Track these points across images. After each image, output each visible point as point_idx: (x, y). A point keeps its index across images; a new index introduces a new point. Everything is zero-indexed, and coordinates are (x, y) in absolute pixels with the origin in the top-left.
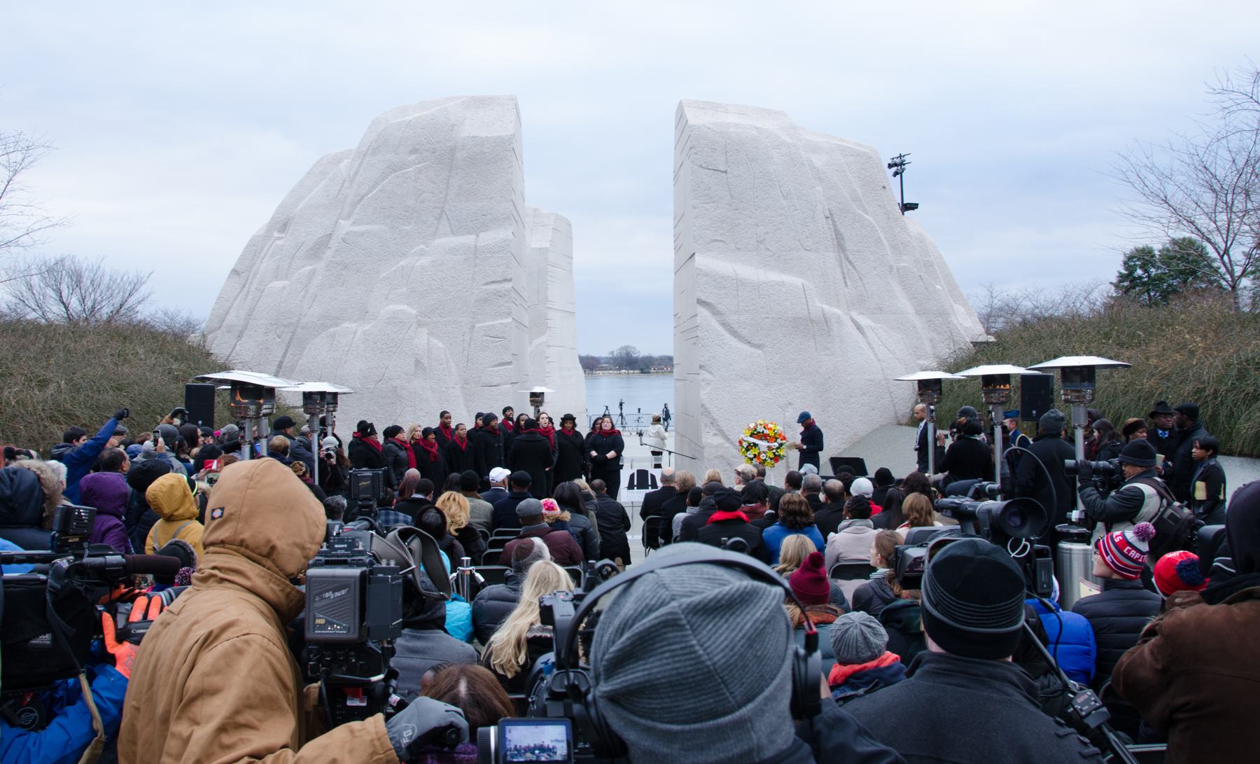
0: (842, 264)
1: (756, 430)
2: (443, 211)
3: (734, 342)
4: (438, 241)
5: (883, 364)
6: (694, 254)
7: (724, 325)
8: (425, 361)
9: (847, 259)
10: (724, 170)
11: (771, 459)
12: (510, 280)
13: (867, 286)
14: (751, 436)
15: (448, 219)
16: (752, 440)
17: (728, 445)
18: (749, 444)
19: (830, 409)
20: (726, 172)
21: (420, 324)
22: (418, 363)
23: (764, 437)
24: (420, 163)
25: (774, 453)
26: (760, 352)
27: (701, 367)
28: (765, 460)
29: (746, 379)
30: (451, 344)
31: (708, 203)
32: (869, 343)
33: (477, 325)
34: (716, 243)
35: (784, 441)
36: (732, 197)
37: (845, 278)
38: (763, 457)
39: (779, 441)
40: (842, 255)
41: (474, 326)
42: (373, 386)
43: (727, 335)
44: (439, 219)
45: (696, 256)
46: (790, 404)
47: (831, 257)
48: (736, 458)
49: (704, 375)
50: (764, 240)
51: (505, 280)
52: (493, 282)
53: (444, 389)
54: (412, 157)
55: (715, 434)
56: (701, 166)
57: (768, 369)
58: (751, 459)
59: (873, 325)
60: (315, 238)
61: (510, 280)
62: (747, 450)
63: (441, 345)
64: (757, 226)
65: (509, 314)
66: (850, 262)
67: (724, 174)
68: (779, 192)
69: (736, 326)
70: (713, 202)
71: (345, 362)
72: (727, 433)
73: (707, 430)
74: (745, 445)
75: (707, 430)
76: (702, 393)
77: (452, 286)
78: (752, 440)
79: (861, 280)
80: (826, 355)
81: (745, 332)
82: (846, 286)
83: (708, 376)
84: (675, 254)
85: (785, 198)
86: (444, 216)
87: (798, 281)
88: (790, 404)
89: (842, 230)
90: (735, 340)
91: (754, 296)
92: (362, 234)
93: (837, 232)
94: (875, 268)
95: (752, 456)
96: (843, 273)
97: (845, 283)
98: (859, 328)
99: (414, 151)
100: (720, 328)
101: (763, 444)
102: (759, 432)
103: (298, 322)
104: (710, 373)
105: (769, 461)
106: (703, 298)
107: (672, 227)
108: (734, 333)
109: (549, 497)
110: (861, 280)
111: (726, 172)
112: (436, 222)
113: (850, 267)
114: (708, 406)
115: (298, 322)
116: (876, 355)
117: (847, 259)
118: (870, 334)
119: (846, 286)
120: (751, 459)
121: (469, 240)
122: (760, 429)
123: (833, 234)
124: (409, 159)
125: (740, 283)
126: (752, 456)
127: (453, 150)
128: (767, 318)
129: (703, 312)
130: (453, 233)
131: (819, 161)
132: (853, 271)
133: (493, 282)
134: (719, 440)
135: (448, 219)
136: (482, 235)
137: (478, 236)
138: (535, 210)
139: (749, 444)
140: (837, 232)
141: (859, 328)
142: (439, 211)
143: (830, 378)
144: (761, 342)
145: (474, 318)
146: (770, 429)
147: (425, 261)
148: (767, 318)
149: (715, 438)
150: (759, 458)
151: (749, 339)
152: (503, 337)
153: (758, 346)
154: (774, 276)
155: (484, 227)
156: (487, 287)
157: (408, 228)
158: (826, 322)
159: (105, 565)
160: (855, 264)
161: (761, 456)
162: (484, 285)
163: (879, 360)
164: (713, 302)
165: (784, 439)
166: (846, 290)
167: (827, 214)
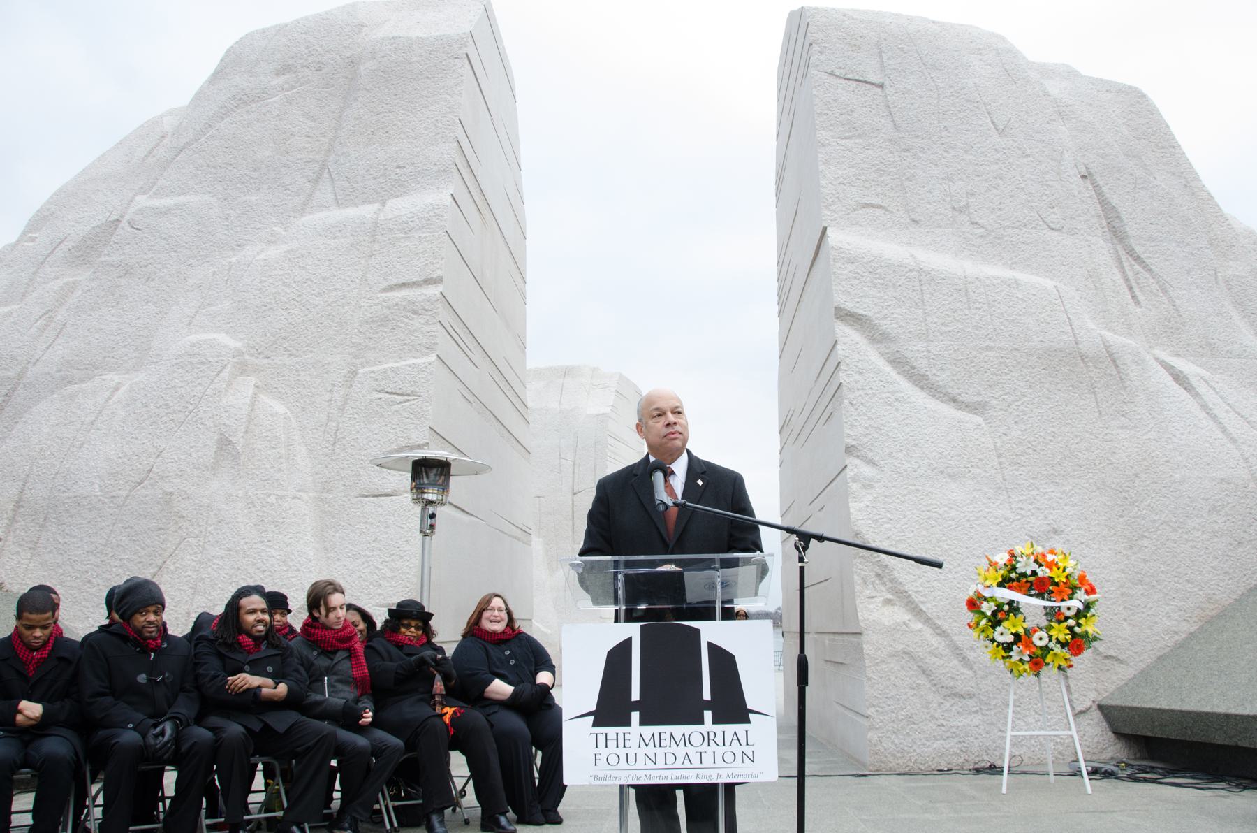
0: (1121, 263)
1: (1014, 569)
2: (324, 165)
3: (921, 398)
4: (308, 219)
5: (1245, 448)
6: (825, 229)
7: (897, 362)
8: (239, 440)
9: (1131, 253)
11: (1064, 645)
13: (1178, 302)
14: (1000, 585)
15: (332, 179)
16: (1005, 594)
17: (919, 626)
18: (999, 606)
19: (1145, 542)
20: (881, 86)
21: (243, 369)
22: (224, 443)
23: (1041, 587)
24: (292, 87)
25: (1070, 628)
26: (978, 419)
27: (849, 450)
28: (1046, 649)
29: (953, 477)
30: (304, 409)
31: (850, 138)
32: (1204, 407)
33: (361, 371)
35: (1092, 597)
36: (896, 127)
37: (1131, 288)
38: (1040, 639)
40: (1119, 248)
41: (355, 373)
42: (124, 493)
43: (905, 385)
44: (316, 181)
45: (829, 232)
46: (1055, 531)
47: (1101, 250)
49: (856, 467)
51: (429, 281)
53: (272, 499)
54: (279, 80)
55: (888, 602)
56: (832, 74)
57: (999, 456)
58: (1008, 647)
59: (1206, 374)
60: (89, 228)
62: (995, 622)
63: (280, 408)
64: (950, 179)
65: (430, 348)
66: (1138, 259)
67: (879, 90)
68: (988, 121)
69: (922, 365)
70: (859, 136)
71: (82, 445)
72: (917, 598)
74: (987, 608)
76: (854, 507)
77: (319, 295)
79: (1165, 291)
80: (1122, 427)
81: (942, 378)
82: (1138, 303)
83: (867, 470)
85: (1001, 133)
86: (326, 175)
87: (1049, 283)
88: (1055, 531)
89: (1115, 201)
90: (923, 394)
92: (166, 212)
93: (1104, 202)
94: (1188, 272)
96: (1127, 280)
97: (1134, 297)
98: (1179, 378)
99: (285, 69)
100: (888, 369)
101: (1032, 605)
102: (1024, 575)
103: (21, 375)
104: (871, 462)
105: (1057, 649)
106: (849, 305)
108: (920, 380)
109: (275, 758)
110: (1165, 291)
111: (881, 86)
112: (309, 186)
113: (1137, 267)
115: (21, 375)
116: (1224, 430)
117: (1131, 253)
118: (1202, 389)
119: (1138, 303)
120: (1008, 647)
122: (1025, 566)
123: (1099, 207)
124: (273, 83)
125: (925, 277)
126: (1010, 639)
127: (353, 63)
128: (989, 348)
129: (848, 336)
130: (338, 204)
131: (1055, 88)
132: (1147, 275)
133: (403, 285)
134: (899, 615)
135: (332, 179)
136: (391, 203)
137: (384, 204)
138: (594, 369)
139: (999, 606)
140: (1104, 202)
141: (1179, 378)
142: (317, 167)
143: (1137, 475)
144: (979, 399)
145: (356, 357)
146: (1051, 565)
147: (273, 252)
149: (887, 610)
151: (955, 392)
152: (413, 393)
153: (973, 408)
155: (398, 188)
156: (389, 294)
157: (253, 198)
158: (1114, 361)
159: (275, 817)
160: (1148, 261)
162: (385, 290)
163: (1234, 441)
166: (1139, 310)
167: (1083, 170)
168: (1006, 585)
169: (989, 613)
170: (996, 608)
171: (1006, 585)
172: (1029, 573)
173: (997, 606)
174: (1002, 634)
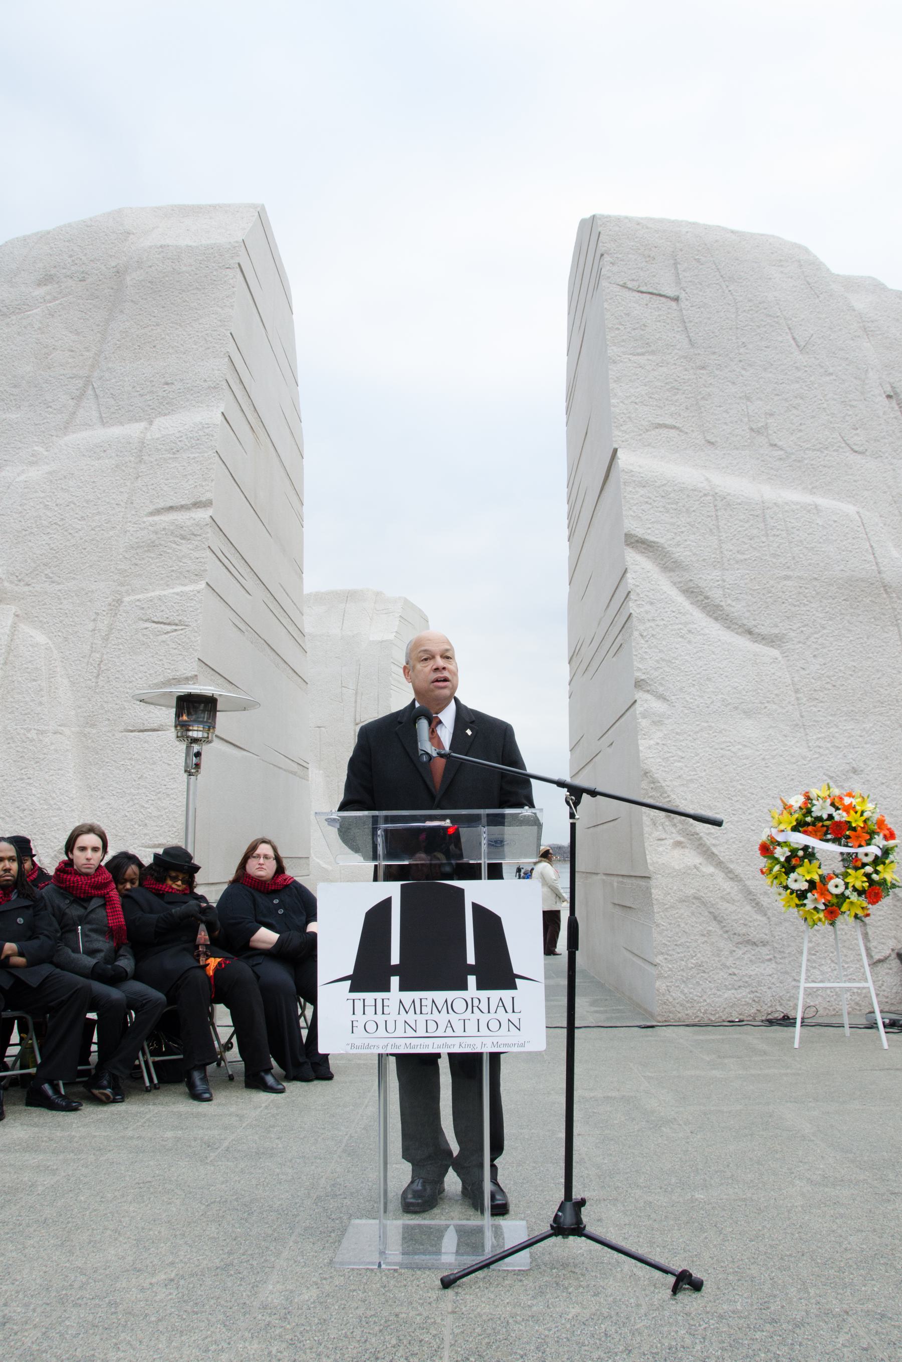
1: (809, 812)
2: (88, 381)
3: (714, 629)
7: (692, 592)
10: (671, 293)
11: (860, 893)
12: (207, 504)
14: (795, 829)
15: (96, 396)
16: (800, 839)
17: (711, 869)
18: (794, 852)
20: (676, 299)
24: (55, 299)
25: (868, 876)
26: (775, 653)
28: (842, 897)
29: (748, 713)
31: (643, 354)
33: (126, 599)
34: (664, 431)
35: (891, 843)
38: (836, 887)
39: (879, 840)
41: (120, 601)
43: (698, 616)
45: (620, 454)
46: (855, 771)
48: (732, 901)
50: (766, 427)
51: (197, 505)
52: (171, 508)
53: (32, 735)
55: (678, 844)
56: (624, 286)
57: (797, 691)
58: (802, 895)
61: (207, 504)
62: (789, 867)
63: (41, 638)
65: (199, 575)
67: (674, 304)
68: (789, 337)
69: (716, 595)
70: (653, 353)
73: (656, 834)
74: (781, 854)
75: (656, 834)
76: (643, 744)
77: (83, 518)
78: (800, 839)
81: (737, 609)
83: (657, 706)
84: (571, 755)
85: (801, 349)
87: (850, 509)
88: (855, 771)
91: (755, 531)
95: (805, 886)
99: (47, 279)
100: (681, 599)
102: (819, 819)
104: (662, 697)
105: (854, 897)
106: (640, 531)
107: (568, 697)
108: (714, 611)
111: (676, 299)
112: (72, 403)
114: (658, 775)
120: (802, 895)
121: (134, 430)
122: (821, 810)
126: (805, 886)
127: (120, 273)
128: (787, 578)
129: (637, 562)
130: (103, 422)
133: (171, 508)
135: (96, 396)
136: (159, 422)
138: (378, 594)
139: (794, 852)
142: (80, 383)
144: (776, 631)
146: (848, 809)
147: (34, 474)
148: (787, 578)
149: (677, 853)
150: (824, 892)
151: (750, 624)
154: (794, 496)
156: (156, 518)
161: (831, 886)
162: (151, 514)
164: (661, 541)
165: (891, 836)
168: (801, 829)
169: (782, 859)
170: (789, 854)
171: (801, 829)
172: (825, 816)
173: (791, 851)
174: (796, 881)
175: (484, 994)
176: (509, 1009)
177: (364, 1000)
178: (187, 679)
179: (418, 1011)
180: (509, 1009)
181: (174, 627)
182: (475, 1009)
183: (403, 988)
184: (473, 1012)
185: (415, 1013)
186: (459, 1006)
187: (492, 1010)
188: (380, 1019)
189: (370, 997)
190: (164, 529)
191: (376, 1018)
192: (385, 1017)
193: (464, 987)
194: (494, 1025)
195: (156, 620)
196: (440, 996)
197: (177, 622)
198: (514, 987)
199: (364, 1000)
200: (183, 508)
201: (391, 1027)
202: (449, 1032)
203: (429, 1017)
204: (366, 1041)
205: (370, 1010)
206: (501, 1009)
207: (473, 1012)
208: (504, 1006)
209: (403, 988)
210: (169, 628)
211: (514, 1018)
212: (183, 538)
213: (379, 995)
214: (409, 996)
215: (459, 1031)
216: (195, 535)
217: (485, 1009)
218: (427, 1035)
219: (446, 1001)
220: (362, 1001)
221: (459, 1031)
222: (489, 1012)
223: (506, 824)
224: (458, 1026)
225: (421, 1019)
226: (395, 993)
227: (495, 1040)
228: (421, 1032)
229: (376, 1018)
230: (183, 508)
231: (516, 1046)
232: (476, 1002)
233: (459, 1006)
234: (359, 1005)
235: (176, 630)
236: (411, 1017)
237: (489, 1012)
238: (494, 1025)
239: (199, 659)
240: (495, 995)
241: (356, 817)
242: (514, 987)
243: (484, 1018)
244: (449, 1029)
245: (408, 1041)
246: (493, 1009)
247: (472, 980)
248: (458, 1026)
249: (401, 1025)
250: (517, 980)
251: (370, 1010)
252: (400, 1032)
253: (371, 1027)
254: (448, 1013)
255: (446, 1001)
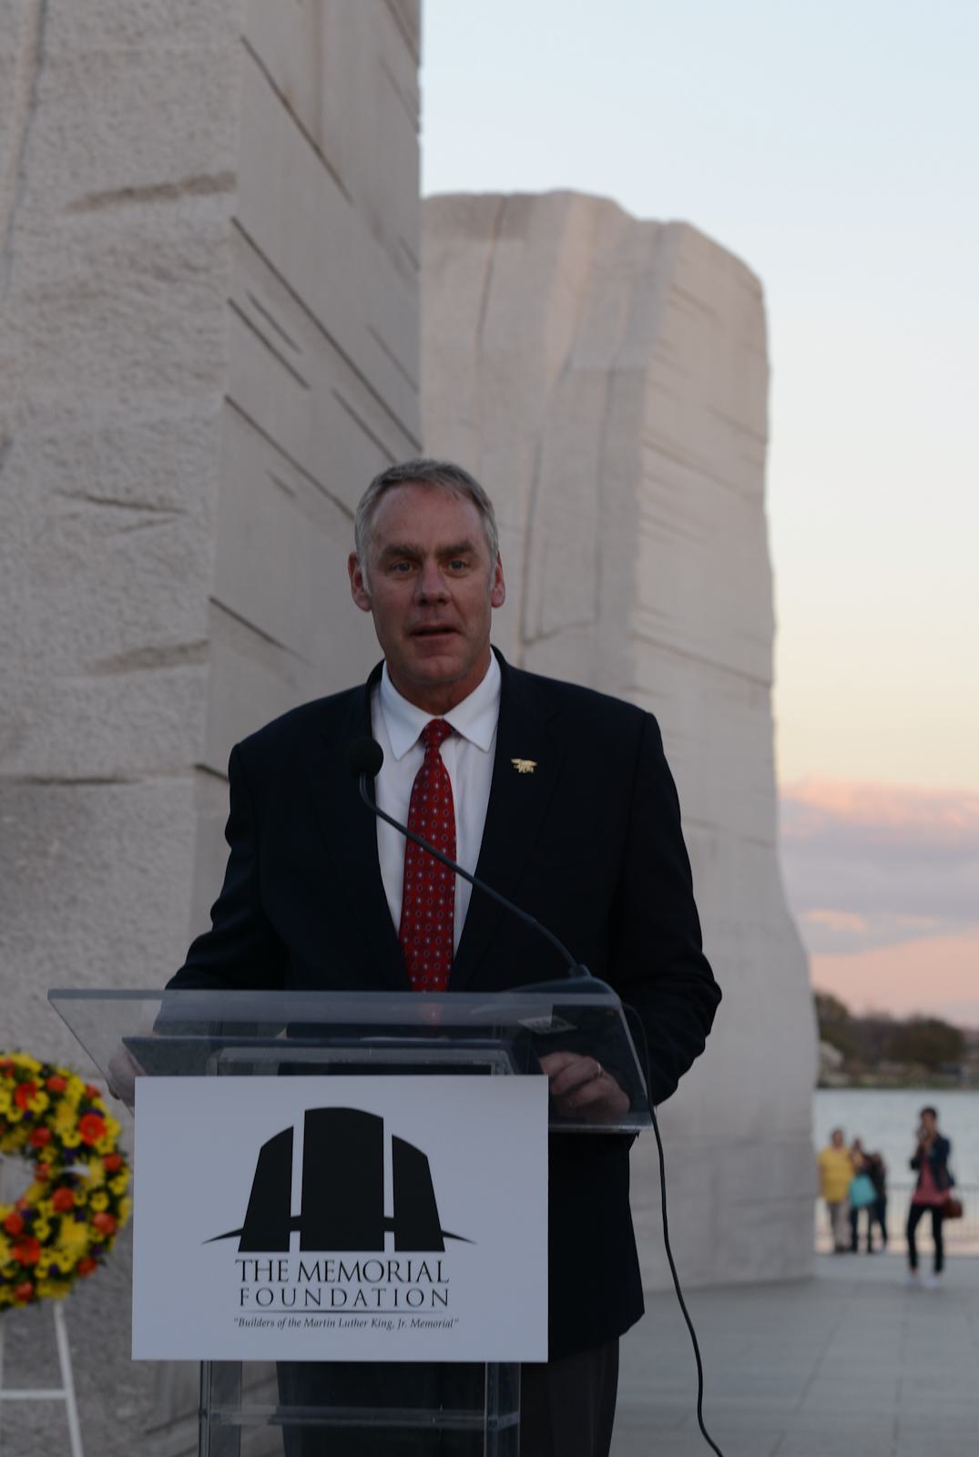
51: (201, 184)
162: (75, 207)
175: (404, 1257)
176: (435, 1277)
177: (257, 1263)
178: (183, 649)
179: (323, 1277)
180: (435, 1277)
181: (146, 515)
182: (393, 1276)
183: (304, 1247)
184: (389, 1280)
185: (319, 1280)
186: (373, 1271)
187: (414, 1277)
188: (276, 1287)
189: (264, 1258)
190: (112, 251)
191: (270, 1285)
192: (282, 1285)
193: (381, 1248)
194: (415, 1298)
195: (97, 493)
196: (350, 1258)
197: (153, 501)
198: (441, 1248)
199: (257, 1263)
200: (164, 192)
201: (288, 1299)
202: (360, 1305)
203: (335, 1285)
204: (259, 1317)
205: (264, 1275)
206: (424, 1278)
207: (389, 1280)
208: (427, 1272)
209: (304, 1247)
210: (129, 517)
211: (440, 1289)
212: (163, 274)
213: (276, 1256)
214: (311, 1258)
215: (372, 1305)
216: (194, 269)
217: (404, 1276)
218: (333, 1308)
219: (357, 1265)
220: (254, 1263)
221: (372, 1305)
222: (409, 1280)
223: (967, 1070)
224: (371, 1298)
225: (326, 1288)
226: (295, 1255)
227: (416, 1317)
228: (326, 1305)
229: (270, 1285)
230: (164, 192)
231: (442, 1325)
232: (394, 1267)
233: (373, 1271)
234: (250, 1268)
235: (150, 523)
236: (313, 1285)
237: (409, 1280)
238: (415, 1298)
239: (213, 601)
240: (418, 1258)
241: (629, 1047)
242: (441, 1248)
243: (403, 1289)
244: (360, 1303)
245: (310, 1316)
246: (414, 1276)
247: (389, 1238)
248: (371, 1298)
249: (301, 1295)
250: (446, 1241)
251: (264, 1275)
252: (300, 1305)
253: (265, 1297)
254: (359, 1279)
255: (357, 1265)
